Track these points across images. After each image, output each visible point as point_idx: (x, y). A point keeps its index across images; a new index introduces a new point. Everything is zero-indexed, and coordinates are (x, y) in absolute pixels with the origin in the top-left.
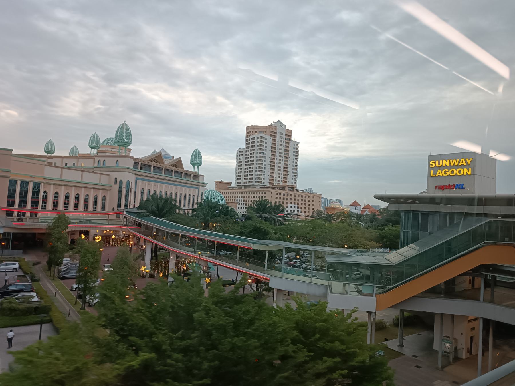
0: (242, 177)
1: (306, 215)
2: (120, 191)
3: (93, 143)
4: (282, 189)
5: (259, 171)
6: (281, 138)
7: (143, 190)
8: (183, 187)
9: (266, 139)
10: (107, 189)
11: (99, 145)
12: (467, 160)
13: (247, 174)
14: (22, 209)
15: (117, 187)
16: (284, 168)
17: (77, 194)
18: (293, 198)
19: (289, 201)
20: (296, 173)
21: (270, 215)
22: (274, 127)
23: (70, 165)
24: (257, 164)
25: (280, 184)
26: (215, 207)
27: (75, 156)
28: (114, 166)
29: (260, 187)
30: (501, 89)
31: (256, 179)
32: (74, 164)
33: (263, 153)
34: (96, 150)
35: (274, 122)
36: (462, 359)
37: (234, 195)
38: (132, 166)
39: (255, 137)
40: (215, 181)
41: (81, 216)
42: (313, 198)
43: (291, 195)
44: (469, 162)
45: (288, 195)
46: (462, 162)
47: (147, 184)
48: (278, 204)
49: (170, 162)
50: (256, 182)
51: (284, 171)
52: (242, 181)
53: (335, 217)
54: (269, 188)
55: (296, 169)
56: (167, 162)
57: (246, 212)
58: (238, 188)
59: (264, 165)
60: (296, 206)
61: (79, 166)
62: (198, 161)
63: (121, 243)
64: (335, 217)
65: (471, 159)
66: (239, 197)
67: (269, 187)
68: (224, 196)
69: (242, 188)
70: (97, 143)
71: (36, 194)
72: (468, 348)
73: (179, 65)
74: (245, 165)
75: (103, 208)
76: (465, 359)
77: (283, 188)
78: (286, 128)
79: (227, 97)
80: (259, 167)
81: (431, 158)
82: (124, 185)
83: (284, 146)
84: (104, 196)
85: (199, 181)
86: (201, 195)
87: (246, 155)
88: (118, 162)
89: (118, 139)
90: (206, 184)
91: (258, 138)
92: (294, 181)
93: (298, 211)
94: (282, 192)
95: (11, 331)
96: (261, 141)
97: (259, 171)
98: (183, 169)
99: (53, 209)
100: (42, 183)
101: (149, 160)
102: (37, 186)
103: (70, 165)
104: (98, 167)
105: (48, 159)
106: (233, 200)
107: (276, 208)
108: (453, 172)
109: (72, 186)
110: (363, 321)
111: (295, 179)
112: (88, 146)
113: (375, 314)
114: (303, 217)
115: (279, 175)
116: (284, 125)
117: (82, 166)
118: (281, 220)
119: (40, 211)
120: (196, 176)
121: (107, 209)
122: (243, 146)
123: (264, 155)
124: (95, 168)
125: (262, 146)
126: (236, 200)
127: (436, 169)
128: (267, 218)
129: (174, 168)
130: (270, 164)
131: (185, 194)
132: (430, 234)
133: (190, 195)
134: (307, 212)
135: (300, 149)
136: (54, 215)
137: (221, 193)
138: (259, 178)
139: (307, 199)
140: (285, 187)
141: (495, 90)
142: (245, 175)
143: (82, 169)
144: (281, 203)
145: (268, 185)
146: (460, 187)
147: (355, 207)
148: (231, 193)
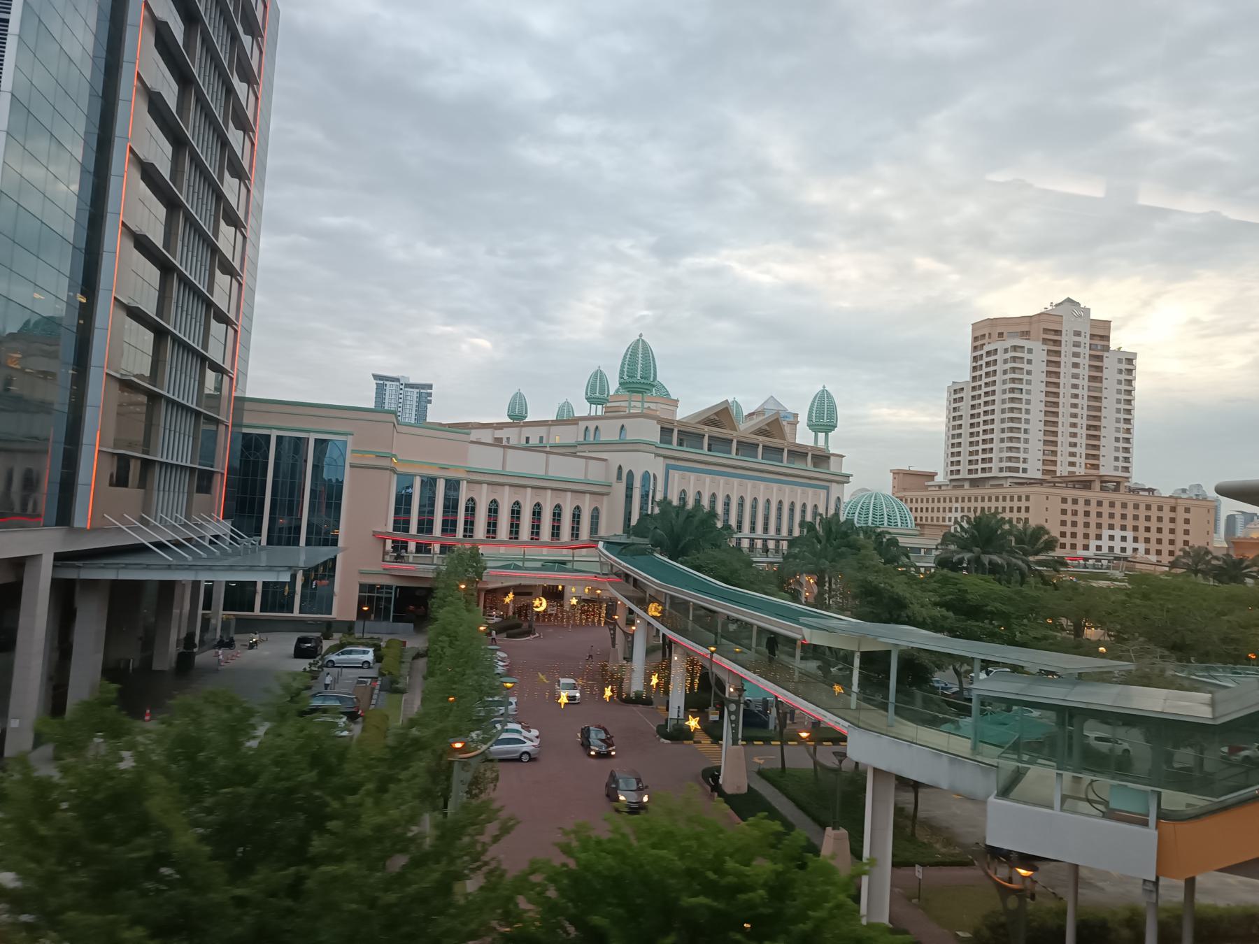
0: (964, 458)
2: (629, 497)
5: (1011, 439)
8: (797, 487)
10: (600, 492)
13: (975, 448)
14: (424, 538)
15: (621, 488)
16: (1089, 427)
17: (494, 501)
20: (1127, 440)
23: (534, 441)
25: (1077, 474)
27: (566, 420)
29: (1016, 483)
31: (1001, 460)
32: (541, 438)
33: (1022, 389)
35: (1054, 305)
38: (656, 438)
39: (996, 350)
40: (891, 471)
41: (547, 554)
42: (1187, 510)
45: (1100, 504)
49: (752, 426)
50: (1001, 470)
52: (964, 468)
54: (1042, 485)
56: (744, 428)
58: (954, 486)
63: (581, 616)
67: (1041, 482)
68: (911, 509)
69: (963, 486)
70: (602, 392)
73: (818, 194)
77: (1086, 484)
78: (1092, 317)
79: (942, 257)
82: (637, 483)
85: (828, 468)
89: (625, 377)
91: (1006, 351)
93: (1135, 550)
94: (1082, 494)
97: (1011, 439)
98: (785, 440)
99: (487, 537)
100: (463, 480)
101: (699, 423)
102: (453, 485)
103: (534, 441)
104: (418, 425)
105: (496, 429)
106: (938, 518)
107: (1027, 539)
109: (525, 487)
110: (1233, 904)
111: (1125, 458)
113: (1154, 889)
114: (1152, 568)
116: (1084, 308)
117: (557, 442)
118: (1046, 573)
120: (821, 458)
122: (965, 376)
124: (578, 446)
128: (997, 564)
129: (761, 439)
137: (901, 500)
138: (1010, 459)
140: (1090, 481)
145: (1039, 476)
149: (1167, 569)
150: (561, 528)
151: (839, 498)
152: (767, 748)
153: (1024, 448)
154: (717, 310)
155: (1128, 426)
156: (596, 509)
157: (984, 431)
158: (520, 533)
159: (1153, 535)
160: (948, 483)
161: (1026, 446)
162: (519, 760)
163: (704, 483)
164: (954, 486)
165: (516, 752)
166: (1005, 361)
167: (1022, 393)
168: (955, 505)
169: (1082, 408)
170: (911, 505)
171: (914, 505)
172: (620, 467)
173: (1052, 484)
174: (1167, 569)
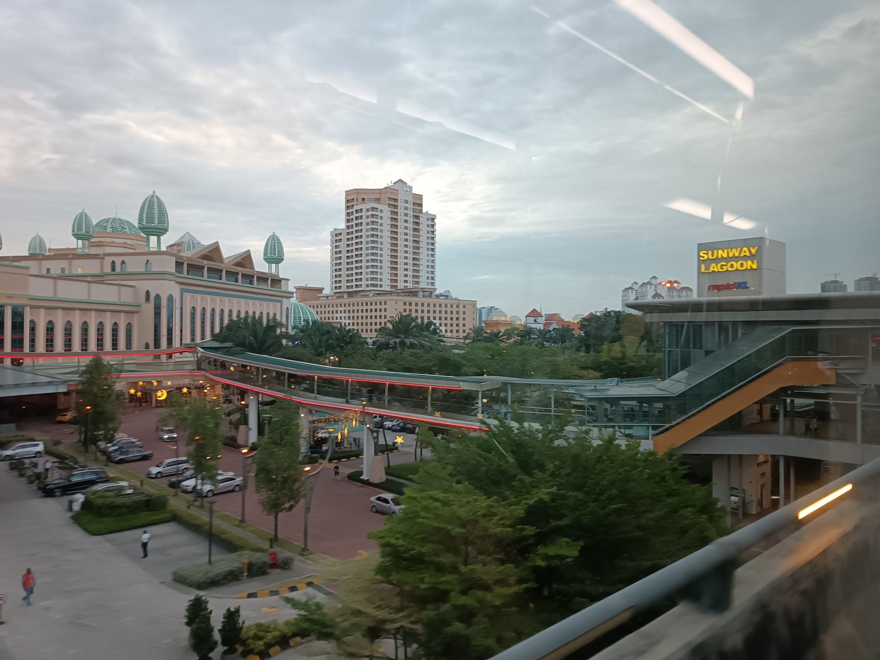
0: (344, 279)
1: (461, 336)
2: (157, 314)
3: (80, 228)
5: (373, 266)
6: (406, 208)
7: (193, 310)
9: (381, 211)
10: (132, 311)
11: (91, 233)
12: (751, 249)
15: (150, 308)
16: (414, 259)
17: (50, 322)
21: (417, 339)
22: (394, 191)
24: (367, 255)
25: (409, 287)
26: (328, 332)
28: (143, 270)
30: (739, 114)
32: (63, 269)
33: (377, 235)
35: (393, 182)
36: (753, 515)
37: (331, 309)
38: (172, 269)
39: (362, 209)
42: (464, 307)
43: (429, 305)
44: (753, 251)
45: (423, 305)
46: (745, 252)
47: (218, 300)
48: (426, 321)
50: (367, 286)
52: (344, 285)
53: (506, 337)
54: (391, 294)
55: (433, 260)
57: (377, 336)
58: (337, 297)
59: (380, 256)
61: (74, 272)
64: (506, 337)
65: (756, 248)
66: (341, 313)
67: (391, 293)
69: (343, 296)
72: (759, 500)
74: (347, 257)
75: (129, 345)
76: (757, 514)
77: (414, 293)
78: (413, 192)
79: (292, 136)
80: (373, 260)
81: (701, 247)
82: (164, 303)
83: (412, 222)
84: (116, 324)
85: (280, 288)
86: (287, 314)
87: (348, 239)
88: (125, 264)
91: (368, 210)
94: (413, 299)
95: (145, 532)
96: (373, 216)
97: (373, 266)
101: (198, 258)
102: (18, 316)
108: (732, 266)
111: (432, 277)
112: (71, 234)
115: (406, 273)
116: (409, 186)
119: (27, 355)
120: (276, 281)
121: (135, 347)
122: (342, 225)
123: (379, 240)
125: (375, 223)
126: (335, 318)
127: (708, 262)
131: (202, 307)
132: (707, 353)
134: (454, 331)
135: (437, 227)
136: (86, 361)
137: (310, 306)
138: (372, 279)
139: (455, 310)
140: (417, 292)
141: (731, 116)
142: (347, 274)
143: (89, 279)
144: (432, 319)
145: (388, 289)
146: (742, 286)
147: (534, 319)
148: (329, 307)
149: (463, 341)
150: (88, 340)
152: (349, 462)
153: (380, 272)
154: (121, 159)
155: (433, 259)
156: (129, 324)
157: (356, 261)
158: (72, 345)
160: (333, 295)
161: (381, 271)
162: (233, 491)
163: (207, 301)
164: (337, 297)
165: (230, 486)
166: (368, 217)
169: (410, 248)
170: (317, 310)
171: (319, 310)
172: (148, 292)
173: (397, 294)
174: (463, 341)
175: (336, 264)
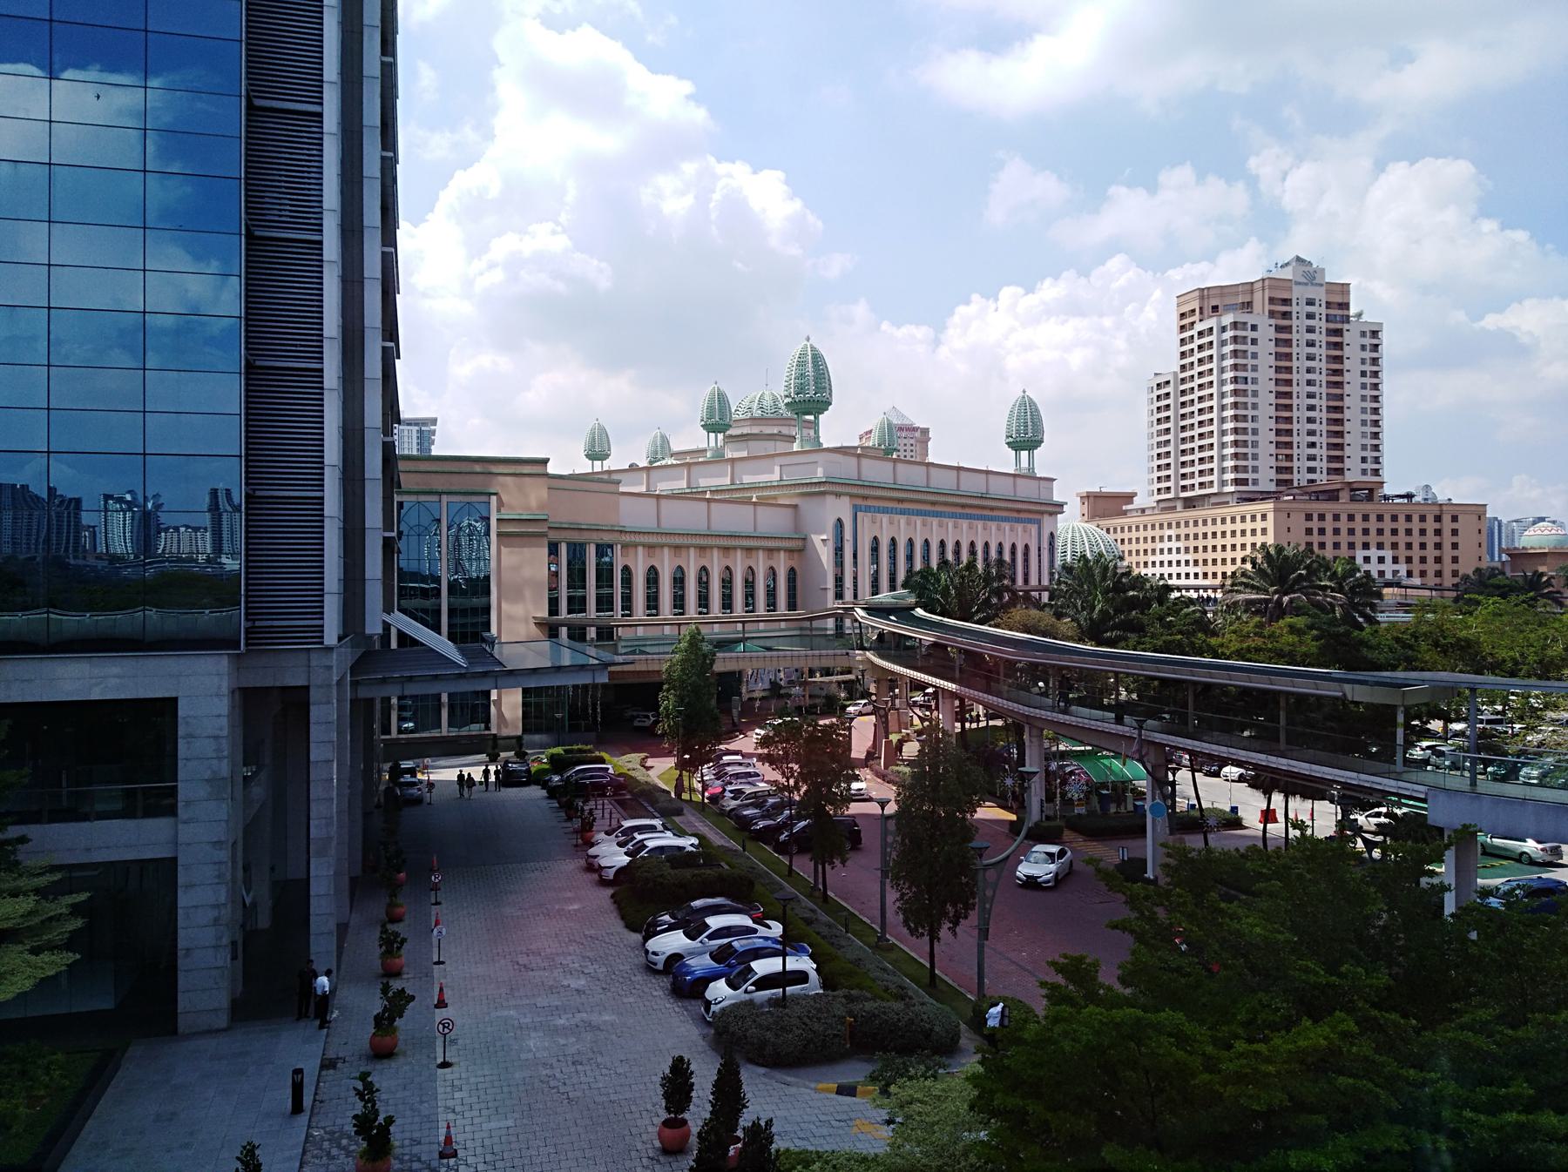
4: (1326, 498)
17: (704, 569)
18: (1373, 525)
19: (1359, 538)
34: (720, 436)
42: (1455, 519)
45: (1351, 518)
51: (1331, 421)
60: (1388, 554)
62: (1030, 431)
69: (1175, 507)
71: (605, 575)
77: (1332, 496)
90: (1061, 505)
92: (1370, 466)
94: (1328, 507)
130: (1274, 414)
133: (1000, 544)
145: (1272, 487)
151: (1052, 534)
159: (1416, 553)
164: (1164, 509)
167: (1246, 383)
168: (1167, 532)
175: (1159, 444)
